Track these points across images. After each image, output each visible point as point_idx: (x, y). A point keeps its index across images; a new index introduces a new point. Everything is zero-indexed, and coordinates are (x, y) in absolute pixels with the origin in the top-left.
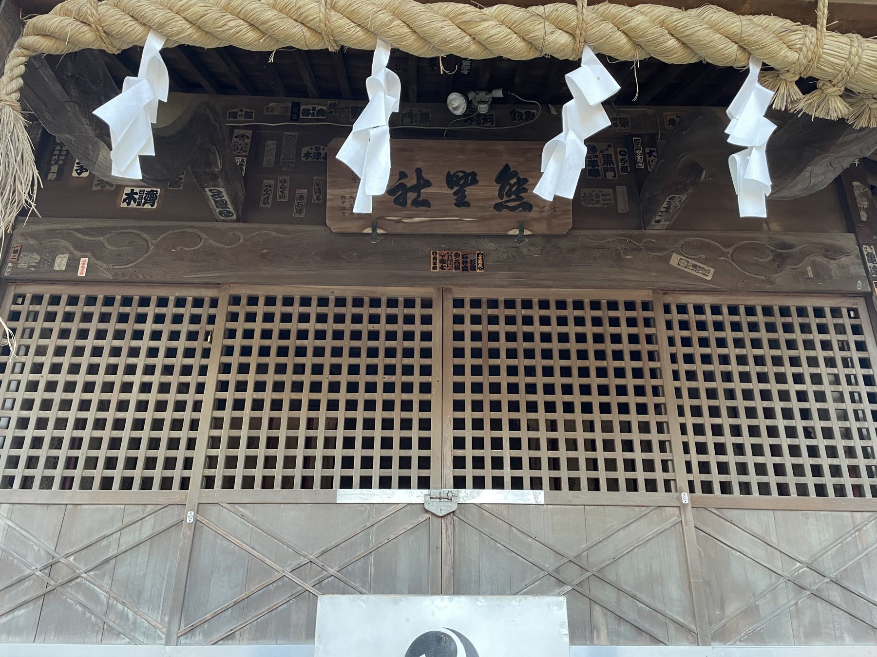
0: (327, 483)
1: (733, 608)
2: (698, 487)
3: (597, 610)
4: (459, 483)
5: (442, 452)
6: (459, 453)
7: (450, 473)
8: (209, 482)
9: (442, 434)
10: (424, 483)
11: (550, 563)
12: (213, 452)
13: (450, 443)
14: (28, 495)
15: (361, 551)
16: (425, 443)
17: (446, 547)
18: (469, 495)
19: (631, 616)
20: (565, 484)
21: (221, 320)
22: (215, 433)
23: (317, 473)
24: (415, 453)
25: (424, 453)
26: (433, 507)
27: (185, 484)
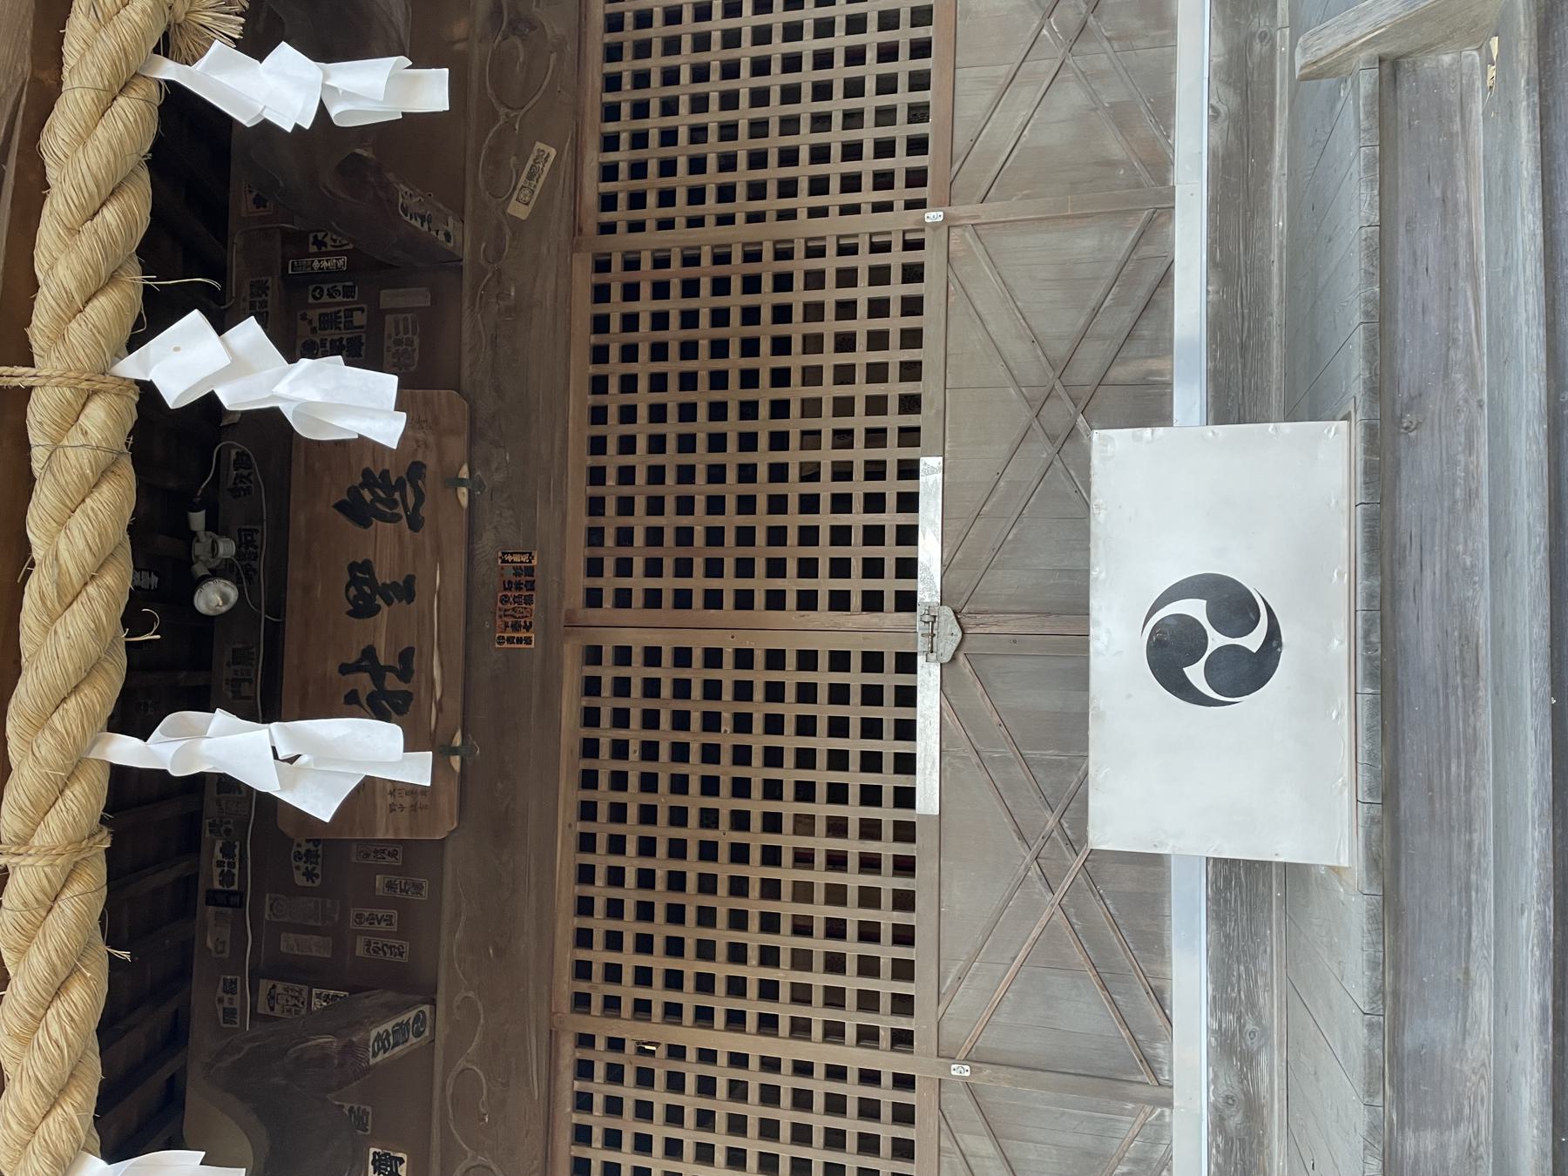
0: (905, 832)
1: (1115, 147)
2: (916, 193)
3: (1119, 373)
4: (907, 602)
5: (856, 631)
6: (856, 601)
7: (889, 618)
8: (902, 1039)
9: (825, 631)
10: (907, 663)
11: (1041, 451)
12: (851, 1033)
13: (839, 617)
15: (1019, 772)
16: (840, 661)
17: (1012, 626)
18: (928, 587)
19: (1126, 317)
20: (910, 420)
21: (616, 1028)
22: (817, 1031)
23: (887, 848)
24: (855, 679)
25: (856, 662)
26: (947, 647)
27: (904, 1082)
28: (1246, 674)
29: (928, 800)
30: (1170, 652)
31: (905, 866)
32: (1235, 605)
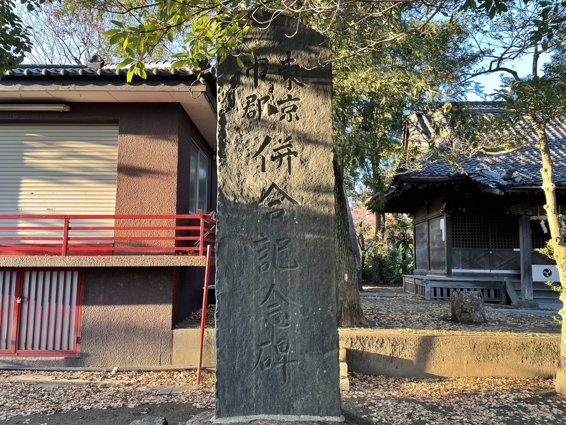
0: (512, 248)
14: (463, 249)
27: (460, 247)
28: (545, 275)
29: (515, 250)
30: (547, 270)
31: (508, 248)
32: (550, 274)
